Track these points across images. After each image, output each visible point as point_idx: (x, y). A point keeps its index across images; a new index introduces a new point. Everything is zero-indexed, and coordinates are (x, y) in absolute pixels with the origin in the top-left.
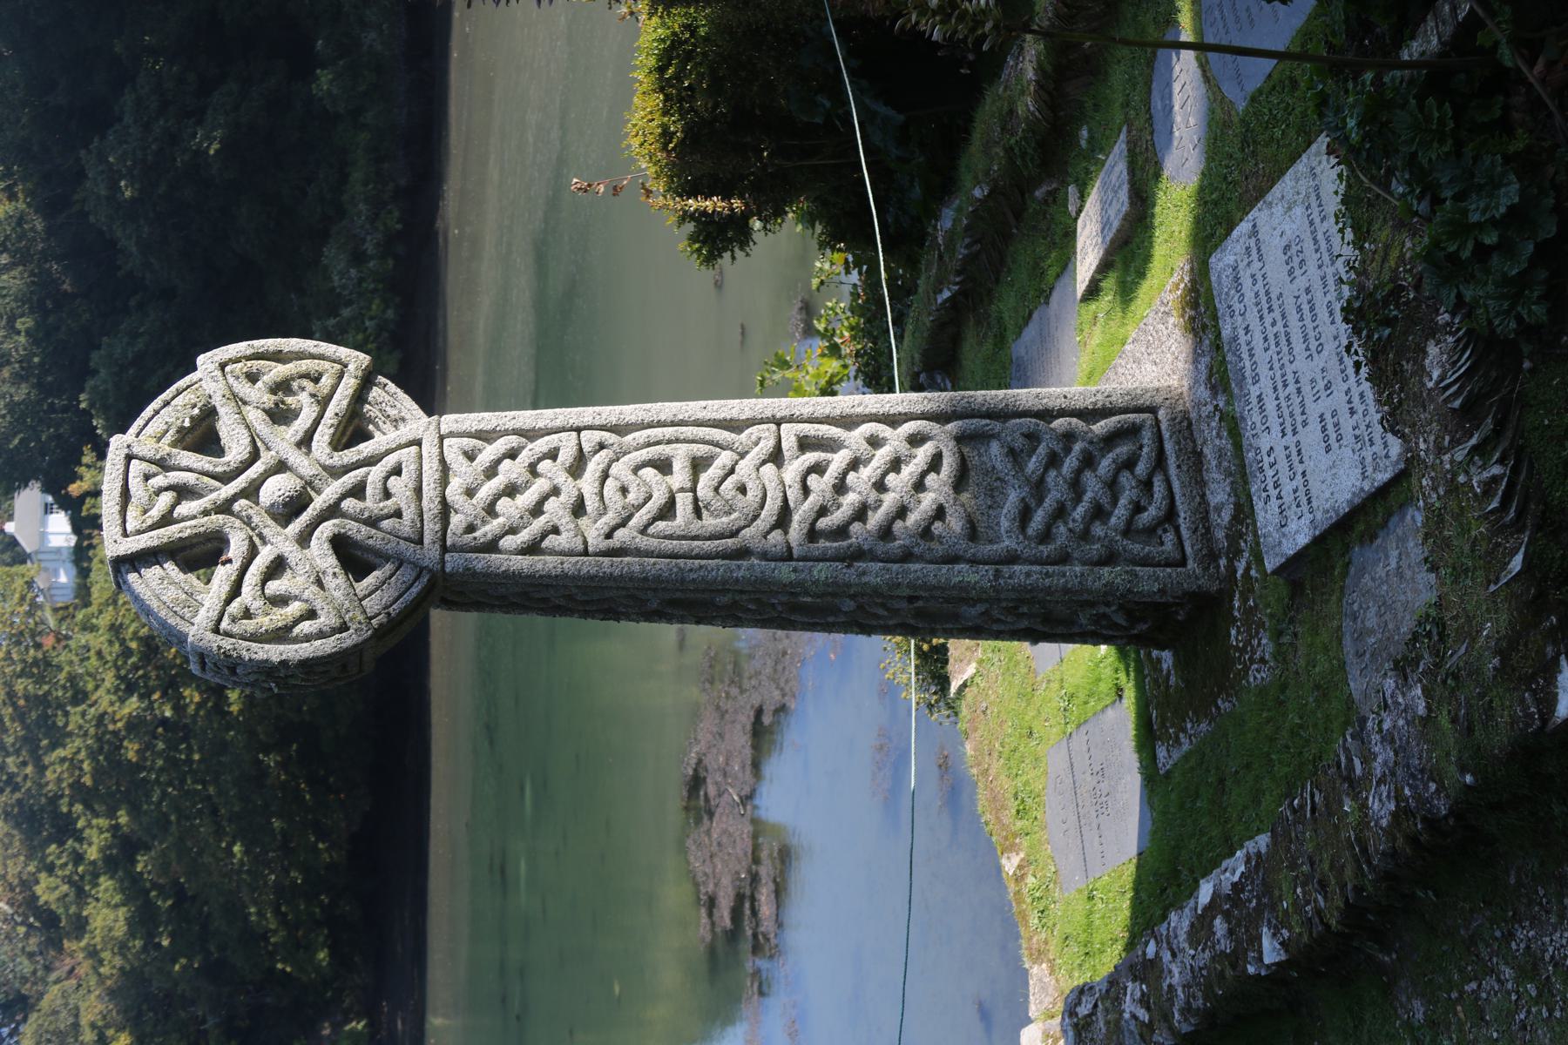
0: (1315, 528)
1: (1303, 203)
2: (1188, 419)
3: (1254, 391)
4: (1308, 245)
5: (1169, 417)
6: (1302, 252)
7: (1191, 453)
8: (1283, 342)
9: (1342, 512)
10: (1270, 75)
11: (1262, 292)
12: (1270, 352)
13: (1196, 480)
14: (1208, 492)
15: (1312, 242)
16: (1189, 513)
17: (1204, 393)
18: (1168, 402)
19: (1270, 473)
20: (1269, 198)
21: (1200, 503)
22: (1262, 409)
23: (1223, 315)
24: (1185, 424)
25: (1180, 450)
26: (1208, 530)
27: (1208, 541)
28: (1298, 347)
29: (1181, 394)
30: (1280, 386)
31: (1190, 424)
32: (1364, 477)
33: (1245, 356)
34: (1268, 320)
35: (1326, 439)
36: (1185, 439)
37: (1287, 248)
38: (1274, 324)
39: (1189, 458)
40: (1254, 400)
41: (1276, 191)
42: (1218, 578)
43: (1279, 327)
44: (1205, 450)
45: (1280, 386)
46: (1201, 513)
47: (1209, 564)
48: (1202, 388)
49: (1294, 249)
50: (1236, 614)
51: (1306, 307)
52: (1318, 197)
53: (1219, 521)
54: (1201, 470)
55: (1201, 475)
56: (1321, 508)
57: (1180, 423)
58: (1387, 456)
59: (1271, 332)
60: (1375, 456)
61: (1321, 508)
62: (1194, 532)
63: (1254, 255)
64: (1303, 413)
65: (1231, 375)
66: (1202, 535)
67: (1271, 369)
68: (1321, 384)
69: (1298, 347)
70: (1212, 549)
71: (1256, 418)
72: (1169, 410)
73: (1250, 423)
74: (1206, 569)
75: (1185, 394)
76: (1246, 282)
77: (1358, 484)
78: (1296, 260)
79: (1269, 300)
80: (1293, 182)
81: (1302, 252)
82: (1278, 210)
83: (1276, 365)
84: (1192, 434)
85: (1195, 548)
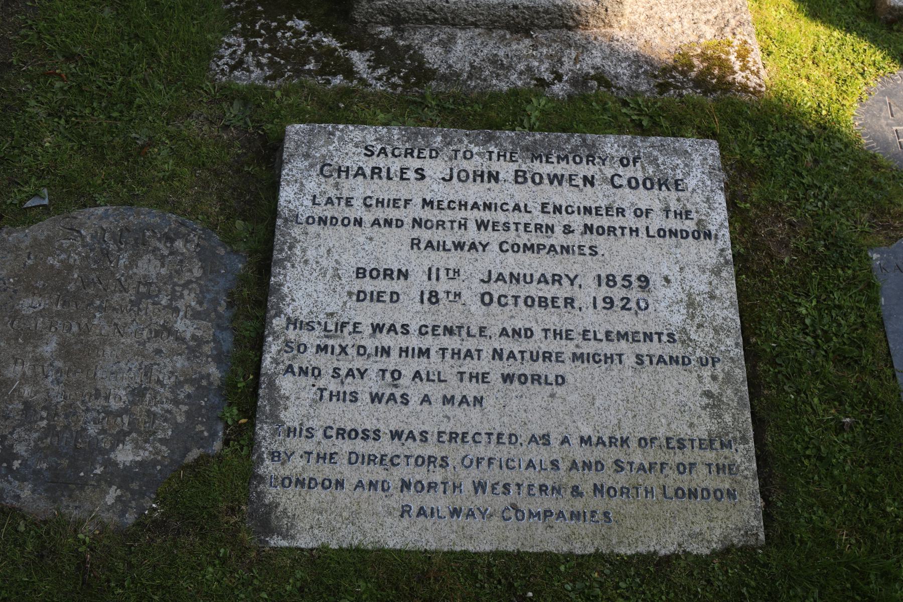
0: (286, 220)
1: (684, 331)
2: (577, 26)
3: (506, 169)
4: (624, 321)
5: (582, 8)
6: (623, 308)
7: (532, 23)
8: (535, 239)
9: (275, 270)
10: (881, 325)
11: (617, 221)
12: (537, 212)
13: (496, 22)
14: (477, 31)
15: (622, 329)
16: (454, 7)
17: (593, 60)
18: (603, 11)
19: (395, 165)
20: (728, 273)
21: (465, 20)
22: (479, 176)
23: (632, 145)
24: (571, 23)
25: (538, 12)
26: (432, 22)
27: (417, 20)
28: (513, 263)
29: (611, 26)
30: (486, 216)
31: (570, 28)
32: (292, 322)
33: (560, 168)
34: (577, 221)
35: (374, 274)
36: (551, 20)
37: (644, 280)
38: (568, 230)
39: (527, 20)
40: (495, 166)
41: (728, 290)
42: (370, 22)
43: (558, 239)
44: (527, 42)
45: (486, 216)
46: (453, 19)
47: (388, 16)
48: (598, 61)
49: (635, 294)
50: (317, 36)
51: (549, 291)
52: (674, 360)
53: (435, 39)
54: (508, 28)
55: (502, 28)
56: (302, 238)
57: (573, 19)
58: (290, 369)
59: (558, 221)
60: (302, 348)
61: (302, 238)
62: (429, 7)
63: (674, 224)
64: (430, 244)
65: (552, 136)
66: (424, 15)
67: (517, 208)
68: (441, 287)
69: (513, 263)
70: (407, 22)
71: (477, 163)
72: (591, 9)
73: (475, 150)
74: (381, 12)
75: (609, 30)
76: (644, 198)
77: (289, 310)
78: (617, 293)
79: (601, 231)
80: (719, 321)
81: (623, 308)
82: (700, 284)
83: (514, 217)
84: (556, 27)
85: (409, 6)
